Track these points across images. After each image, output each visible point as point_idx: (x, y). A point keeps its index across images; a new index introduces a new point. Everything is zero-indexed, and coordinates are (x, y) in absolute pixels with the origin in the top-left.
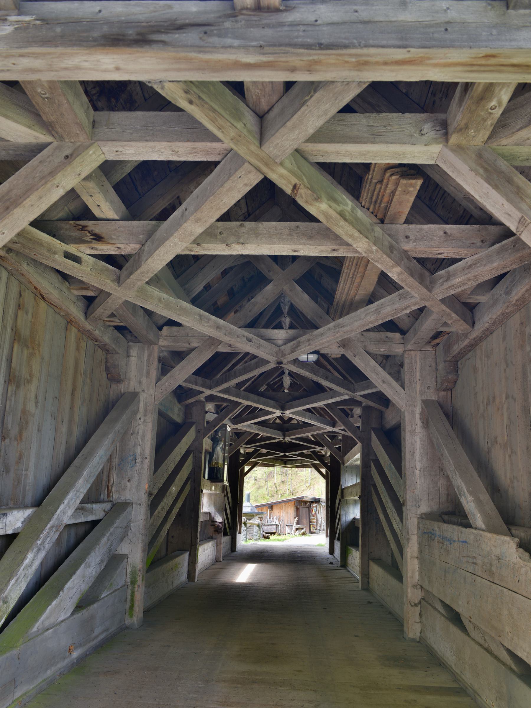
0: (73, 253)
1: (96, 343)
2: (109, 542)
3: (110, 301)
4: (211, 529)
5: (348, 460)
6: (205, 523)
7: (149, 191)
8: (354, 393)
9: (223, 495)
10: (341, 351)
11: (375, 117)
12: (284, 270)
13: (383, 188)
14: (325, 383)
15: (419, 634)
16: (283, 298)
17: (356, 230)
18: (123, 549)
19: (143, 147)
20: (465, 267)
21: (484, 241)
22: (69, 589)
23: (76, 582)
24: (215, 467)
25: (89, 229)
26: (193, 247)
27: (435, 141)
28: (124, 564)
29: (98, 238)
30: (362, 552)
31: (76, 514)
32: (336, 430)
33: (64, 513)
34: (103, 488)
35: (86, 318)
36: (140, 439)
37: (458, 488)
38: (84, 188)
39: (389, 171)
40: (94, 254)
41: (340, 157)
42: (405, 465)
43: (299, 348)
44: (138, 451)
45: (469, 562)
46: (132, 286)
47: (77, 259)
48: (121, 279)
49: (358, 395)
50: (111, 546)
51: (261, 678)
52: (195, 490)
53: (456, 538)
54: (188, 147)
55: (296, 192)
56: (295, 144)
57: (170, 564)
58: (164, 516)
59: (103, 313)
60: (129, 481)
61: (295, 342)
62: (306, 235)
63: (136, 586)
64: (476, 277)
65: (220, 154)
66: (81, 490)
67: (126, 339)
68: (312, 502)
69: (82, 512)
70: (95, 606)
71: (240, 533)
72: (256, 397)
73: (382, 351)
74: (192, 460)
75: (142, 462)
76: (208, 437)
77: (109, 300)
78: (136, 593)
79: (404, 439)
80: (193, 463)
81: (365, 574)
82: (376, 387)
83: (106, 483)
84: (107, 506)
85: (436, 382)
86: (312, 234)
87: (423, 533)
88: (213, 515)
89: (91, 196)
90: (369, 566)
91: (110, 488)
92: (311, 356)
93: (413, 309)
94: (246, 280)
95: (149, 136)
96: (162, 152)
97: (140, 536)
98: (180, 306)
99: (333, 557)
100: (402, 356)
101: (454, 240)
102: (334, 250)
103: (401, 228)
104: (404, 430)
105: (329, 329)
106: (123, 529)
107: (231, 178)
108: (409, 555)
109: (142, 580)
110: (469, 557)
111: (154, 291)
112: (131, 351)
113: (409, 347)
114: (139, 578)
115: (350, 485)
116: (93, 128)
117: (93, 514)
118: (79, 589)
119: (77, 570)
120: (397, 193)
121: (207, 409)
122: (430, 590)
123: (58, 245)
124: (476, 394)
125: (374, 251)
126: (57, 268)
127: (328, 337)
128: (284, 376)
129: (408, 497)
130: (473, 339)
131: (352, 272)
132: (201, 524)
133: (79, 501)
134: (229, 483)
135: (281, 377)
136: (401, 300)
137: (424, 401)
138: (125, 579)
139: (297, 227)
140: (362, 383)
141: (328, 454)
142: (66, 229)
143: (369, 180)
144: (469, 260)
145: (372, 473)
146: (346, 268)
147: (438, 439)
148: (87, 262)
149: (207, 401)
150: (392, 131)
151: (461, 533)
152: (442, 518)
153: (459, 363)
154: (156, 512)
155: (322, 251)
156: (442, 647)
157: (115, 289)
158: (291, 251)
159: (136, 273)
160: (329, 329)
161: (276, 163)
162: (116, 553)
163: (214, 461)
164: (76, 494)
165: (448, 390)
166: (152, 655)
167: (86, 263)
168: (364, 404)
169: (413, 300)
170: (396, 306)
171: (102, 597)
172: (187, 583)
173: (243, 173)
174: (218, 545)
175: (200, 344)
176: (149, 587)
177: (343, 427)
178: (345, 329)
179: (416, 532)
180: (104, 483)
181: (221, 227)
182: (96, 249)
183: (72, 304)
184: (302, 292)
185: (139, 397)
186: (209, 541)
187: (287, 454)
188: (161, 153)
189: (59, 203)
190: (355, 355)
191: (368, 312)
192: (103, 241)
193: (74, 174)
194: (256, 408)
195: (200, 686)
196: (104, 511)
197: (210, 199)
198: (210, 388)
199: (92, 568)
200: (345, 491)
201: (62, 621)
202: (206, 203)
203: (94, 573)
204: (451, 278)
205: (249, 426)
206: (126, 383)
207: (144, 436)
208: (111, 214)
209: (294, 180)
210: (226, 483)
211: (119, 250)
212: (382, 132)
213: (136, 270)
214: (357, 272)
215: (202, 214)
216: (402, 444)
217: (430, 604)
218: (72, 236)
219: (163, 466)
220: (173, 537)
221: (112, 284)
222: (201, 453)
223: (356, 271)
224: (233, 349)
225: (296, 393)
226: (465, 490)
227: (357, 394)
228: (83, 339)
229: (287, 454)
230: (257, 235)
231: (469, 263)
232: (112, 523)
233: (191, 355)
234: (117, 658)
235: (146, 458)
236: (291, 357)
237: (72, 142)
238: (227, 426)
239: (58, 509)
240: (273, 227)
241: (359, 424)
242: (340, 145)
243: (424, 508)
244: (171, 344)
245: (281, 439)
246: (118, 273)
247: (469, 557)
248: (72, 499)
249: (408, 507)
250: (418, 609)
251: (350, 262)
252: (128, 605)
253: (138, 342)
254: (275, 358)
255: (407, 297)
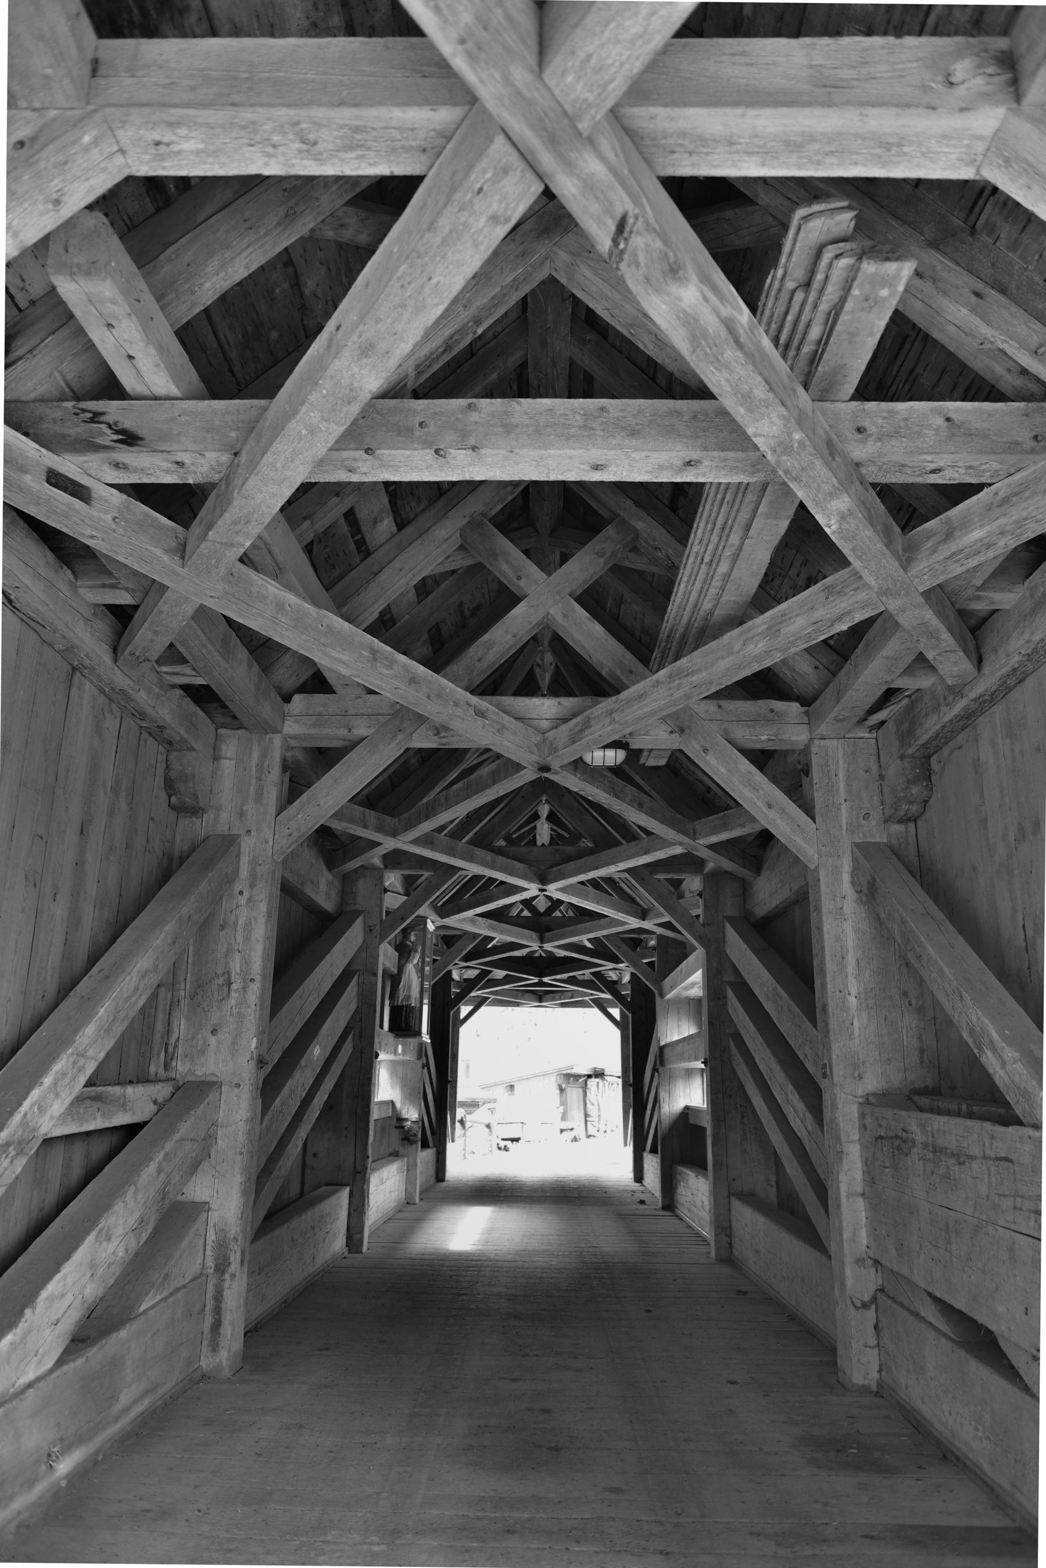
0: (71, 476)
1: (144, 724)
2: (162, 1176)
3: (165, 608)
4: (395, 1135)
5: (672, 988)
6: (383, 1122)
7: (258, 377)
8: (694, 839)
9: (420, 1064)
10: (674, 742)
11: (828, 45)
12: (549, 574)
13: (811, 299)
14: (636, 817)
15: (877, 1376)
16: (540, 655)
17: (760, 379)
18: (199, 1190)
19: (223, 128)
20: (992, 504)
21: (1039, 438)
22: (52, 1299)
23: (69, 1281)
24: (403, 1006)
25: (107, 418)
26: (355, 460)
27: (987, 98)
28: (199, 1224)
29: (130, 439)
30: (715, 1179)
31: (82, 1111)
32: (647, 925)
33: (42, 1110)
34: (156, 1049)
35: (115, 660)
36: (240, 938)
37: (972, 1032)
38: (90, 301)
39: (830, 247)
40: (121, 482)
41: (736, 157)
42: (824, 986)
43: (587, 732)
44: (236, 965)
45: (1021, 1209)
46: (213, 561)
47: (79, 491)
48: (188, 547)
49: (702, 845)
50: (167, 1184)
51: (526, 1516)
52: (362, 1052)
53: (975, 1151)
54: (342, 127)
55: (622, 246)
56: (637, 58)
57: (309, 1217)
58: (294, 1110)
59: (152, 641)
60: (214, 1032)
61: (579, 719)
62: (624, 428)
63: (227, 1276)
64: (1020, 523)
65: (424, 150)
66: (91, 1052)
67: (213, 722)
68: (589, 1076)
69: (97, 1105)
70: (123, 1333)
71: (453, 1141)
72: (489, 856)
73: (763, 742)
74: (355, 989)
75: (244, 988)
76: (390, 943)
77: (163, 606)
78: (227, 1293)
79: (820, 928)
80: (358, 995)
81: (724, 1227)
82: (753, 819)
83: (163, 1037)
84: (162, 1091)
85: (882, 803)
86: (637, 424)
87: (876, 1140)
88: (398, 1105)
89: (110, 326)
90: (730, 1210)
91: (170, 1049)
92: (610, 753)
93: (857, 621)
94: (467, 613)
95: (239, 92)
96: (275, 146)
97: (239, 1158)
98: (328, 626)
99: (642, 1188)
100: (806, 750)
101: (971, 435)
102: (689, 463)
103: (847, 410)
104: (818, 909)
105: (658, 683)
106: (196, 1144)
107: (457, 196)
108: (843, 1188)
109: (242, 1262)
110: (1022, 1197)
111: (269, 586)
112: (224, 747)
113: (823, 729)
114: (235, 1258)
115: (676, 1038)
116: (94, 76)
117: (126, 1111)
118: (80, 1297)
119: (75, 1248)
120: (849, 306)
121: (387, 884)
122: (905, 1272)
123: (33, 452)
124: (984, 821)
125: (796, 445)
126: (31, 510)
127: (655, 700)
128: (538, 824)
129: (834, 1057)
130: (975, 700)
131: (711, 547)
132: (375, 1125)
133: (83, 1079)
134: (431, 1038)
135: (532, 825)
136: (831, 598)
137: (858, 845)
138: (200, 1261)
139: (603, 409)
140: (710, 818)
141: (627, 978)
142: (55, 421)
143: (776, 285)
144: (1001, 488)
145: (730, 1010)
146: (697, 541)
147: (903, 922)
148: (106, 501)
149: (386, 867)
150: (874, 78)
151: (992, 1137)
152: (915, 1103)
153: (934, 760)
154: (278, 1101)
155: (661, 468)
156: (947, 1413)
157: (177, 574)
158: (586, 467)
159: (220, 522)
160: (658, 683)
161: (580, 134)
162: (180, 1198)
163: (401, 994)
164: (75, 1063)
165: (909, 820)
166: (258, 1455)
167: (103, 503)
168: (710, 866)
169: (861, 596)
170: (819, 613)
171: (142, 1309)
172: (346, 1254)
173: (488, 175)
174: (411, 1169)
175: (372, 731)
176: (259, 1274)
177: (667, 918)
178: (694, 678)
179: (857, 1137)
180: (157, 1038)
181: (422, 411)
182: (126, 467)
183: (81, 621)
184: (588, 619)
185: (240, 845)
186: (392, 1162)
187: (546, 980)
188: (270, 149)
189: (42, 363)
190: (706, 750)
191: (751, 634)
192: (141, 446)
193: (41, 198)
194: (491, 880)
195: (376, 1548)
196: (155, 1102)
197: (399, 274)
198: (394, 834)
199: (115, 1242)
200: (667, 1051)
201: (30, 1385)
202: (387, 289)
203: (121, 1254)
204: (957, 534)
205: (472, 921)
206: (212, 816)
207: (250, 932)
208: (161, 382)
209: (623, 203)
210: (426, 1038)
211: (181, 471)
212: (846, 80)
213: (221, 516)
214: (724, 548)
215: (379, 326)
216: (814, 941)
217: (901, 1305)
218: (69, 436)
219: (293, 1003)
220: (315, 1155)
221: (166, 558)
222: (375, 974)
223: (722, 544)
224: (444, 741)
225: (569, 848)
226: (995, 1035)
227: (701, 842)
228: (111, 711)
229: (546, 980)
230: (508, 429)
231: (1002, 494)
232: (172, 1129)
233: (352, 755)
234: (171, 1469)
235: (253, 980)
236: (569, 755)
237: (35, 110)
238: (428, 921)
239: (25, 1098)
240: (546, 411)
241: (699, 911)
242: (739, 111)
243: (872, 1082)
244: (311, 731)
245: (535, 946)
246: (181, 536)
247: (1022, 1197)
248: (64, 1075)
249: (836, 1079)
250: (871, 1314)
251: (707, 523)
252: (209, 1320)
253: (239, 728)
254: (535, 758)
255: (846, 590)
